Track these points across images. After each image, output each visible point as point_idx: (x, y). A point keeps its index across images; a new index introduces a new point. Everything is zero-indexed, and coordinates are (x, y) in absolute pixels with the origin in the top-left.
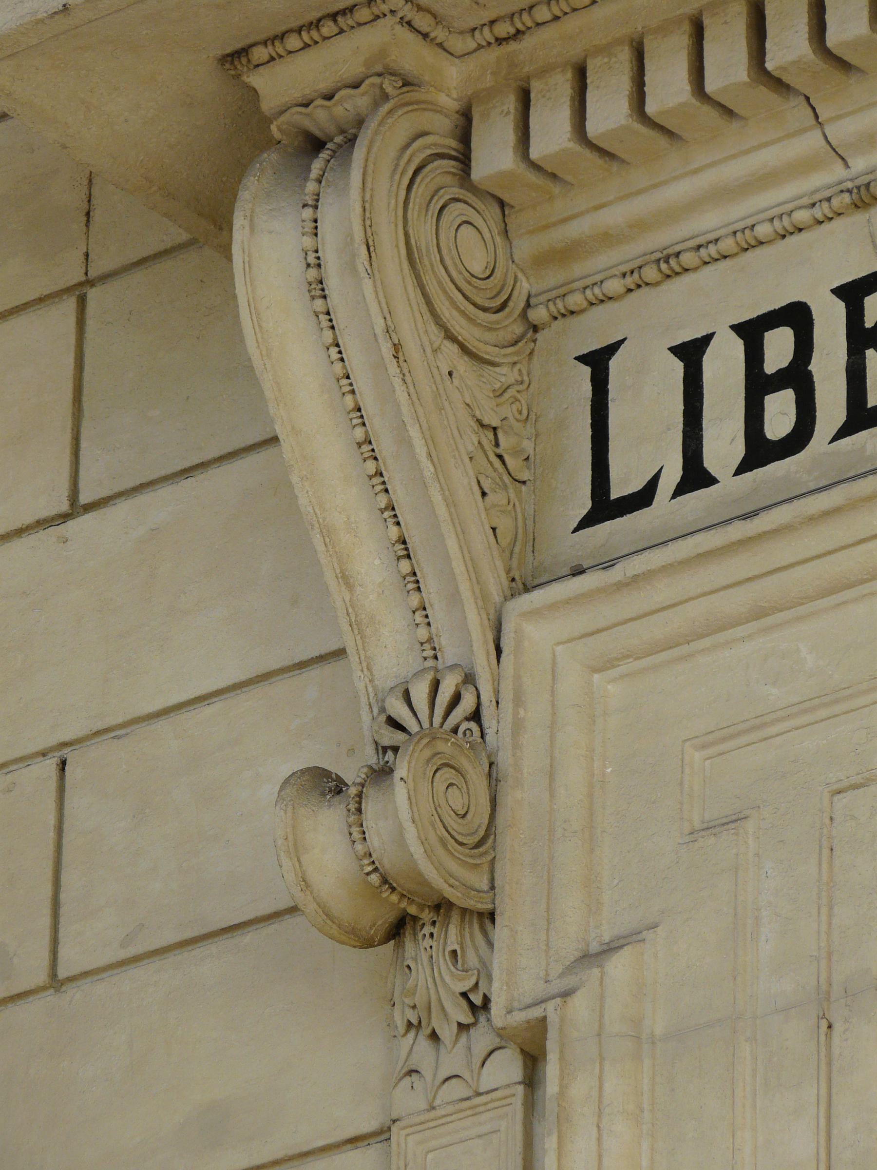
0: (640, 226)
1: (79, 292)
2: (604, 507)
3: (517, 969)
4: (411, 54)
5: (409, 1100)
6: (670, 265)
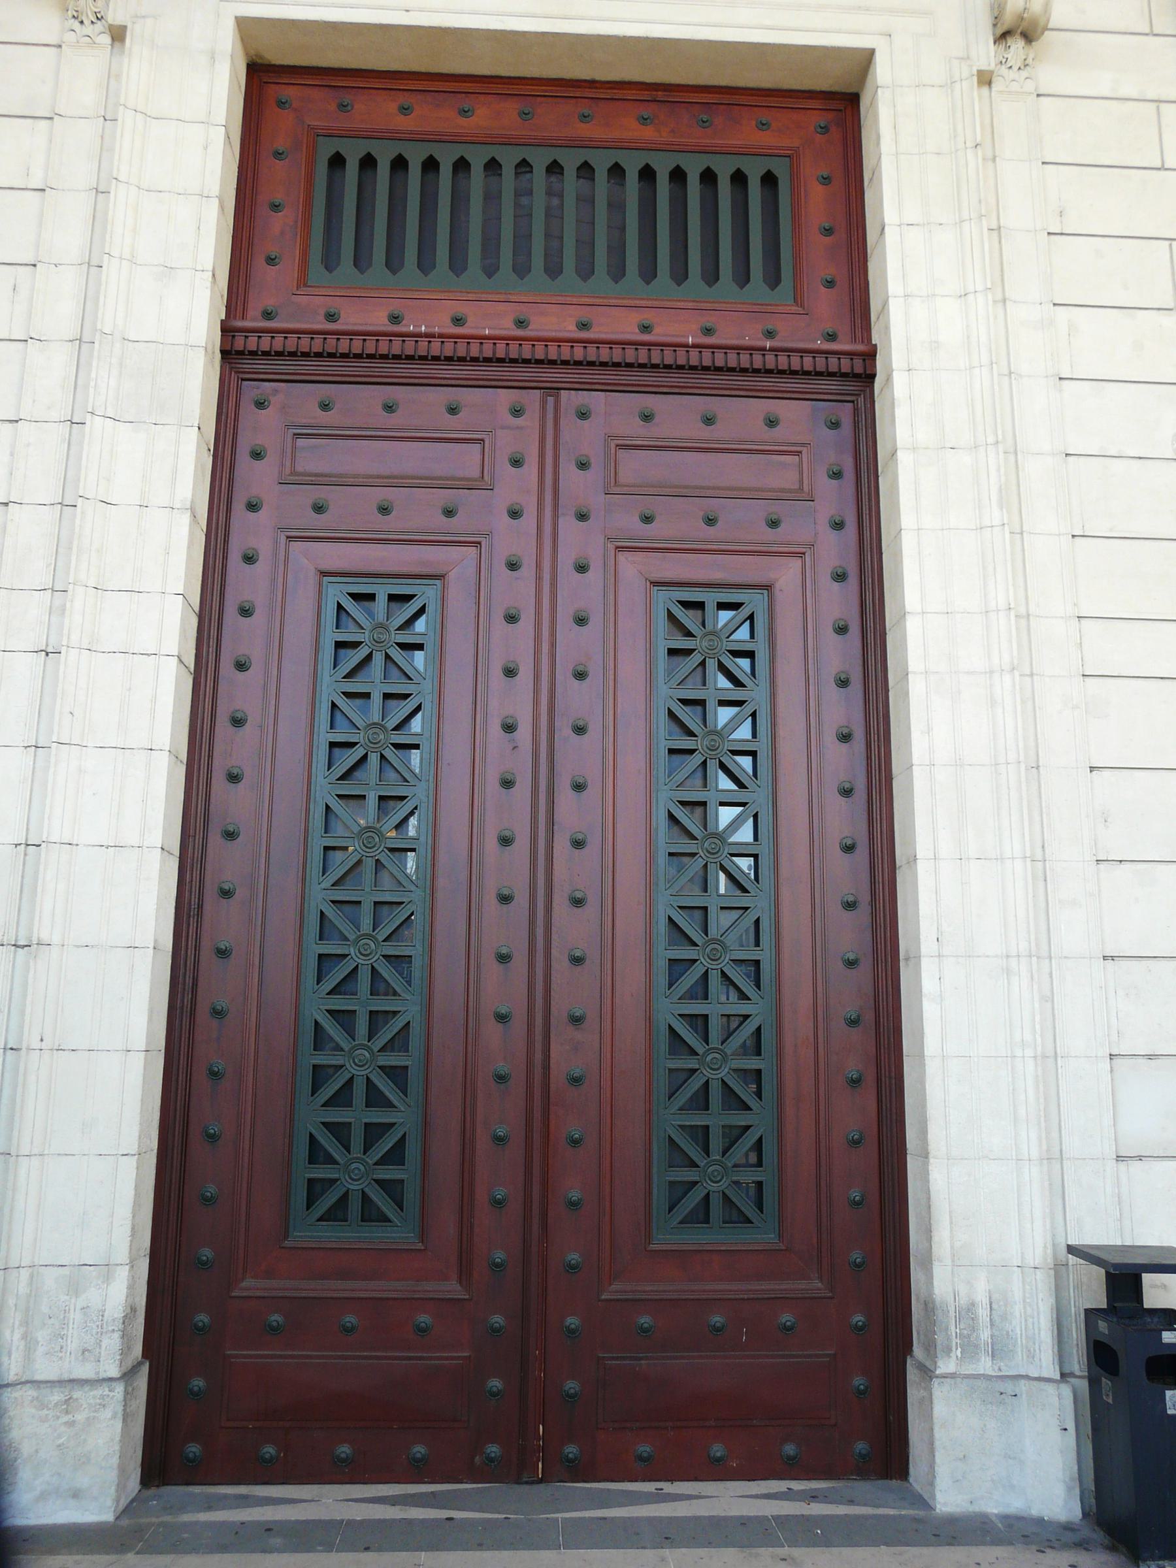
5: (70, 37)
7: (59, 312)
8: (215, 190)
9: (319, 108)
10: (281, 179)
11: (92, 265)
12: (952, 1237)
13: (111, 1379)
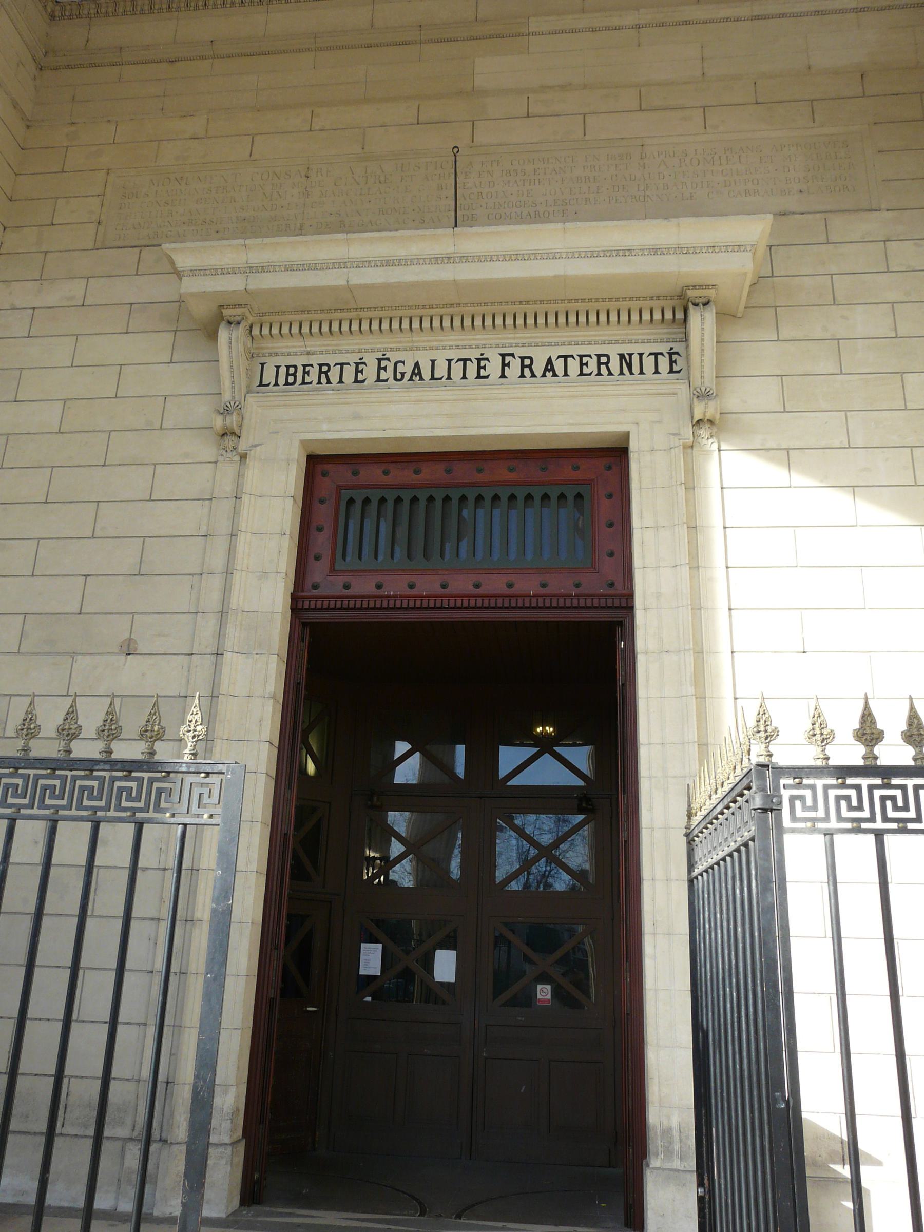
0: (273, 348)
1: (175, 331)
2: (261, 385)
3: (243, 446)
4: (248, 314)
5: (220, 459)
6: (276, 354)
7: (212, 598)
8: (259, 817)
9: (343, 474)
10: (323, 513)
11: (228, 573)
12: (659, 1090)
13: (226, 1144)
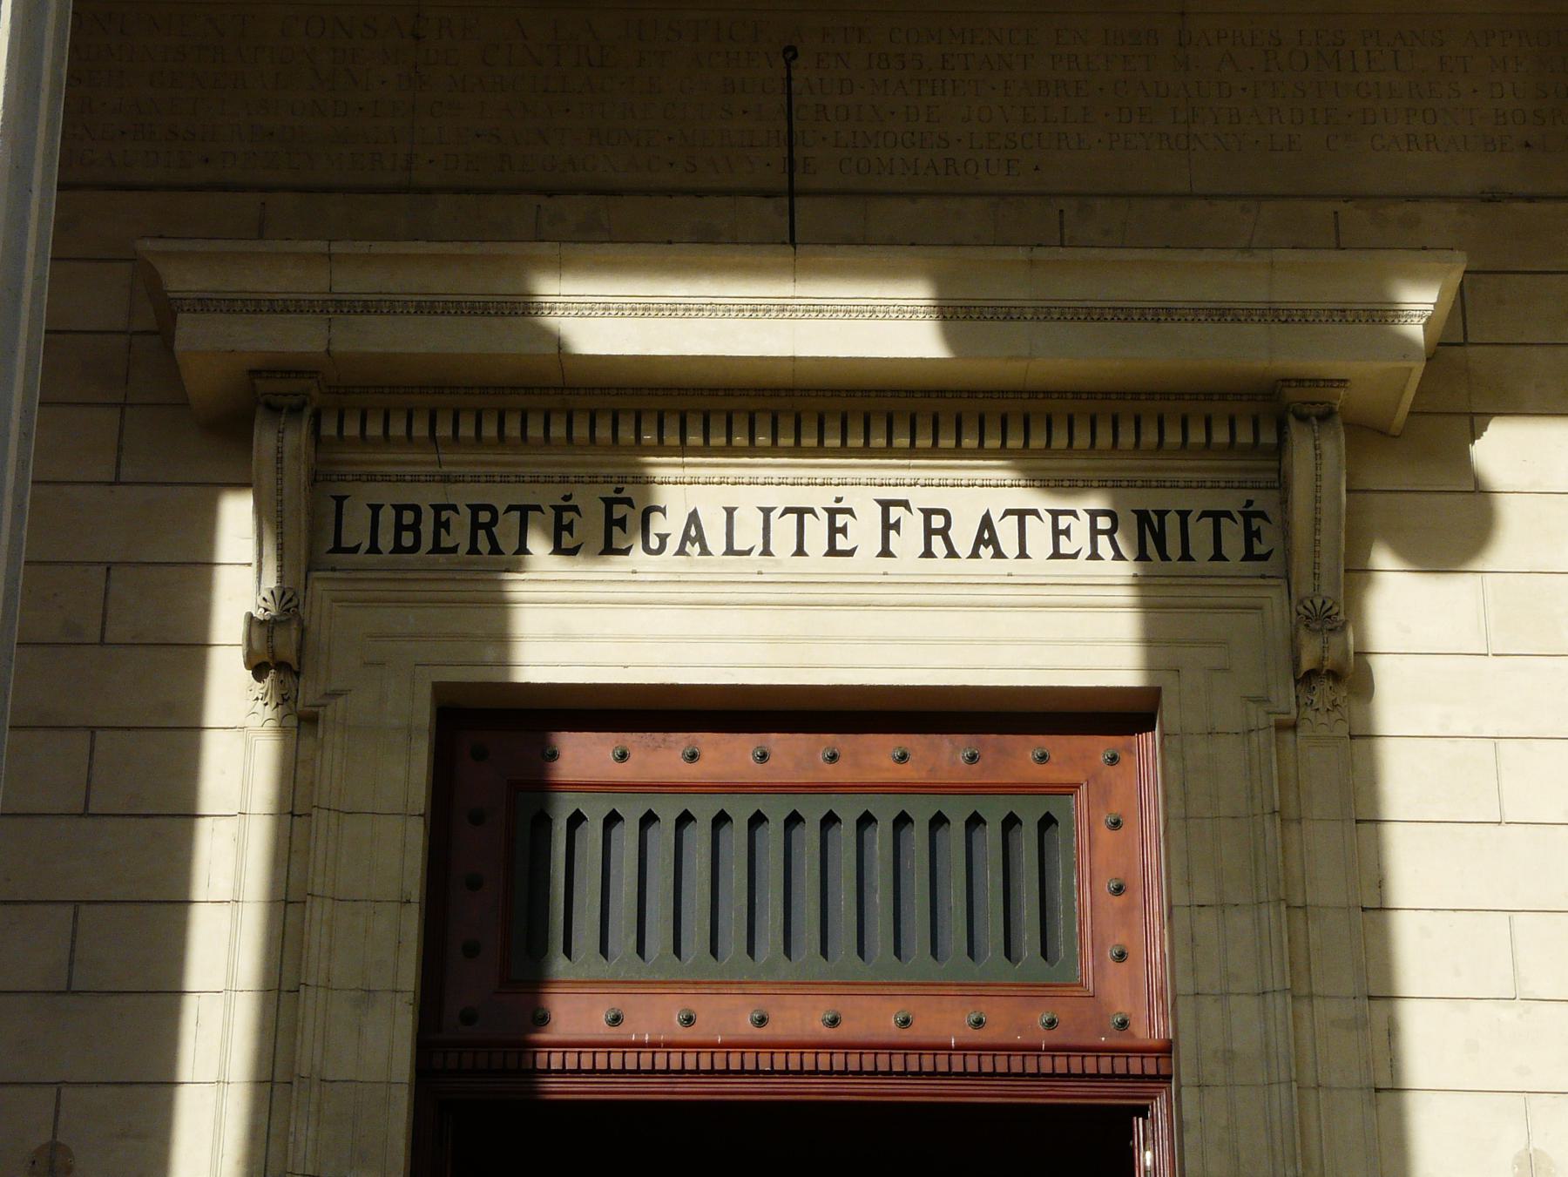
0: (363, 463)
1: (122, 406)
2: (338, 548)
